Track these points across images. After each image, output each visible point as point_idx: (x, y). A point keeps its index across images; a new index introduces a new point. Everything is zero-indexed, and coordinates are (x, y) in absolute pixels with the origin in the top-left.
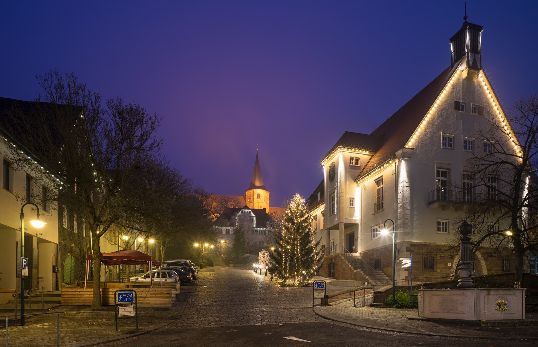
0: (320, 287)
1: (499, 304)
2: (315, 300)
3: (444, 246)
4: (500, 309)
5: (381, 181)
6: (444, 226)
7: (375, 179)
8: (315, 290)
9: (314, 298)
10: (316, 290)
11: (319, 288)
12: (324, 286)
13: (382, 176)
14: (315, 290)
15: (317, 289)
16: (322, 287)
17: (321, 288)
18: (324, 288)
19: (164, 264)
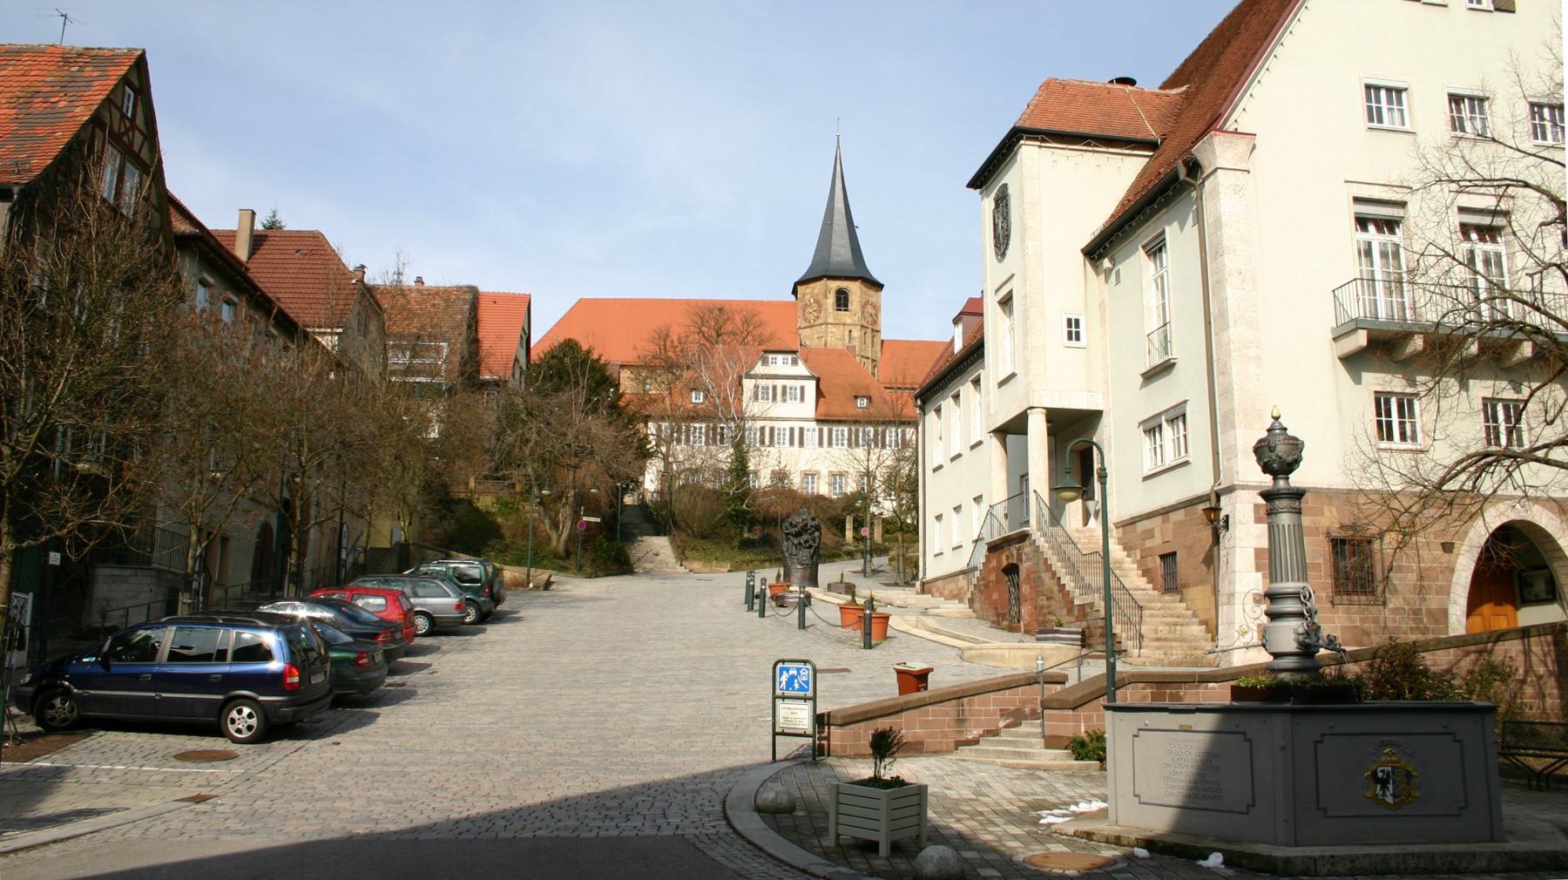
0: (796, 686)
1: (1380, 775)
2: (1533, 426)
3: (967, 368)
4: (1384, 795)
5: (1181, 419)
6: (1387, 421)
7: (1086, 239)
8: (779, 697)
9: (778, 730)
10: (784, 698)
11: (793, 690)
12: (807, 683)
13: (1186, 402)
14: (779, 697)
15: (787, 693)
16: (801, 688)
17: (798, 690)
18: (807, 690)
19: (1147, 541)
